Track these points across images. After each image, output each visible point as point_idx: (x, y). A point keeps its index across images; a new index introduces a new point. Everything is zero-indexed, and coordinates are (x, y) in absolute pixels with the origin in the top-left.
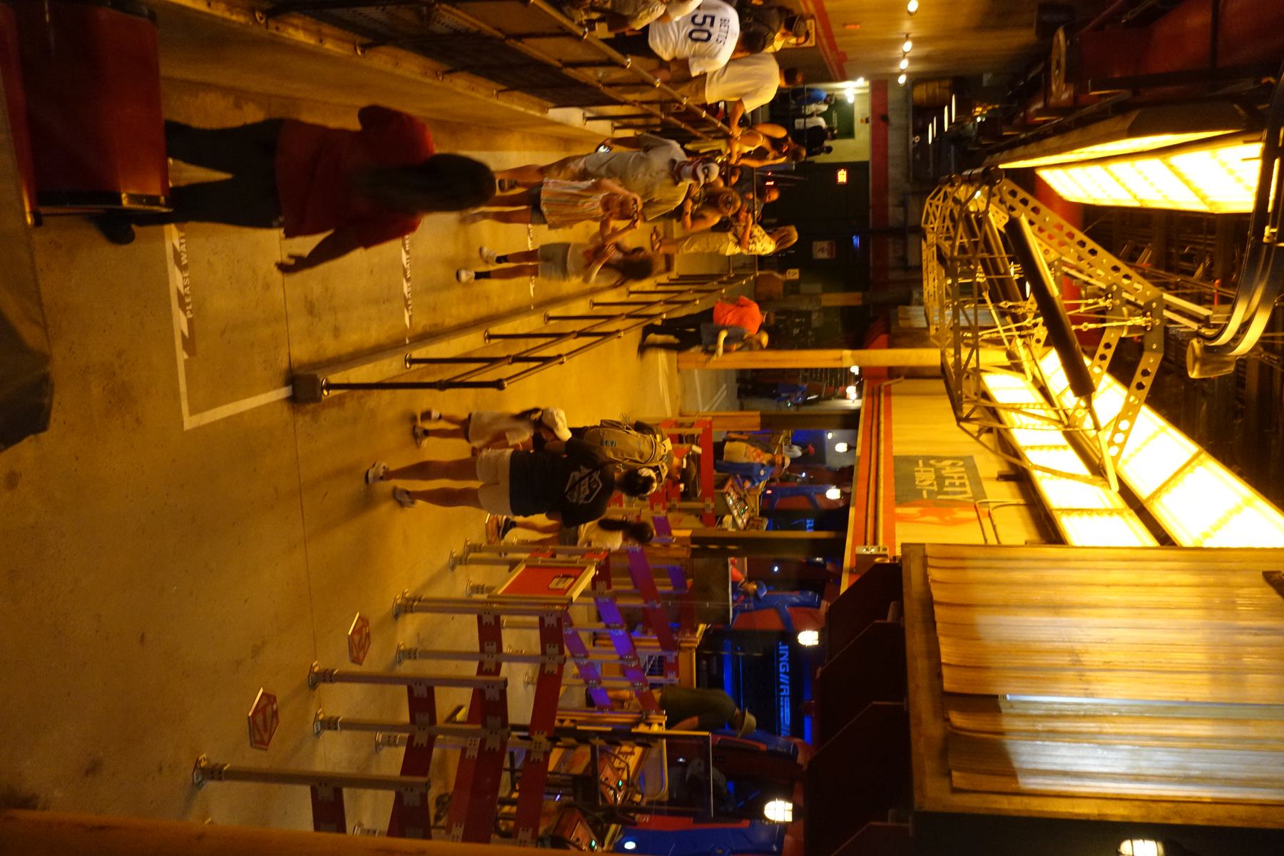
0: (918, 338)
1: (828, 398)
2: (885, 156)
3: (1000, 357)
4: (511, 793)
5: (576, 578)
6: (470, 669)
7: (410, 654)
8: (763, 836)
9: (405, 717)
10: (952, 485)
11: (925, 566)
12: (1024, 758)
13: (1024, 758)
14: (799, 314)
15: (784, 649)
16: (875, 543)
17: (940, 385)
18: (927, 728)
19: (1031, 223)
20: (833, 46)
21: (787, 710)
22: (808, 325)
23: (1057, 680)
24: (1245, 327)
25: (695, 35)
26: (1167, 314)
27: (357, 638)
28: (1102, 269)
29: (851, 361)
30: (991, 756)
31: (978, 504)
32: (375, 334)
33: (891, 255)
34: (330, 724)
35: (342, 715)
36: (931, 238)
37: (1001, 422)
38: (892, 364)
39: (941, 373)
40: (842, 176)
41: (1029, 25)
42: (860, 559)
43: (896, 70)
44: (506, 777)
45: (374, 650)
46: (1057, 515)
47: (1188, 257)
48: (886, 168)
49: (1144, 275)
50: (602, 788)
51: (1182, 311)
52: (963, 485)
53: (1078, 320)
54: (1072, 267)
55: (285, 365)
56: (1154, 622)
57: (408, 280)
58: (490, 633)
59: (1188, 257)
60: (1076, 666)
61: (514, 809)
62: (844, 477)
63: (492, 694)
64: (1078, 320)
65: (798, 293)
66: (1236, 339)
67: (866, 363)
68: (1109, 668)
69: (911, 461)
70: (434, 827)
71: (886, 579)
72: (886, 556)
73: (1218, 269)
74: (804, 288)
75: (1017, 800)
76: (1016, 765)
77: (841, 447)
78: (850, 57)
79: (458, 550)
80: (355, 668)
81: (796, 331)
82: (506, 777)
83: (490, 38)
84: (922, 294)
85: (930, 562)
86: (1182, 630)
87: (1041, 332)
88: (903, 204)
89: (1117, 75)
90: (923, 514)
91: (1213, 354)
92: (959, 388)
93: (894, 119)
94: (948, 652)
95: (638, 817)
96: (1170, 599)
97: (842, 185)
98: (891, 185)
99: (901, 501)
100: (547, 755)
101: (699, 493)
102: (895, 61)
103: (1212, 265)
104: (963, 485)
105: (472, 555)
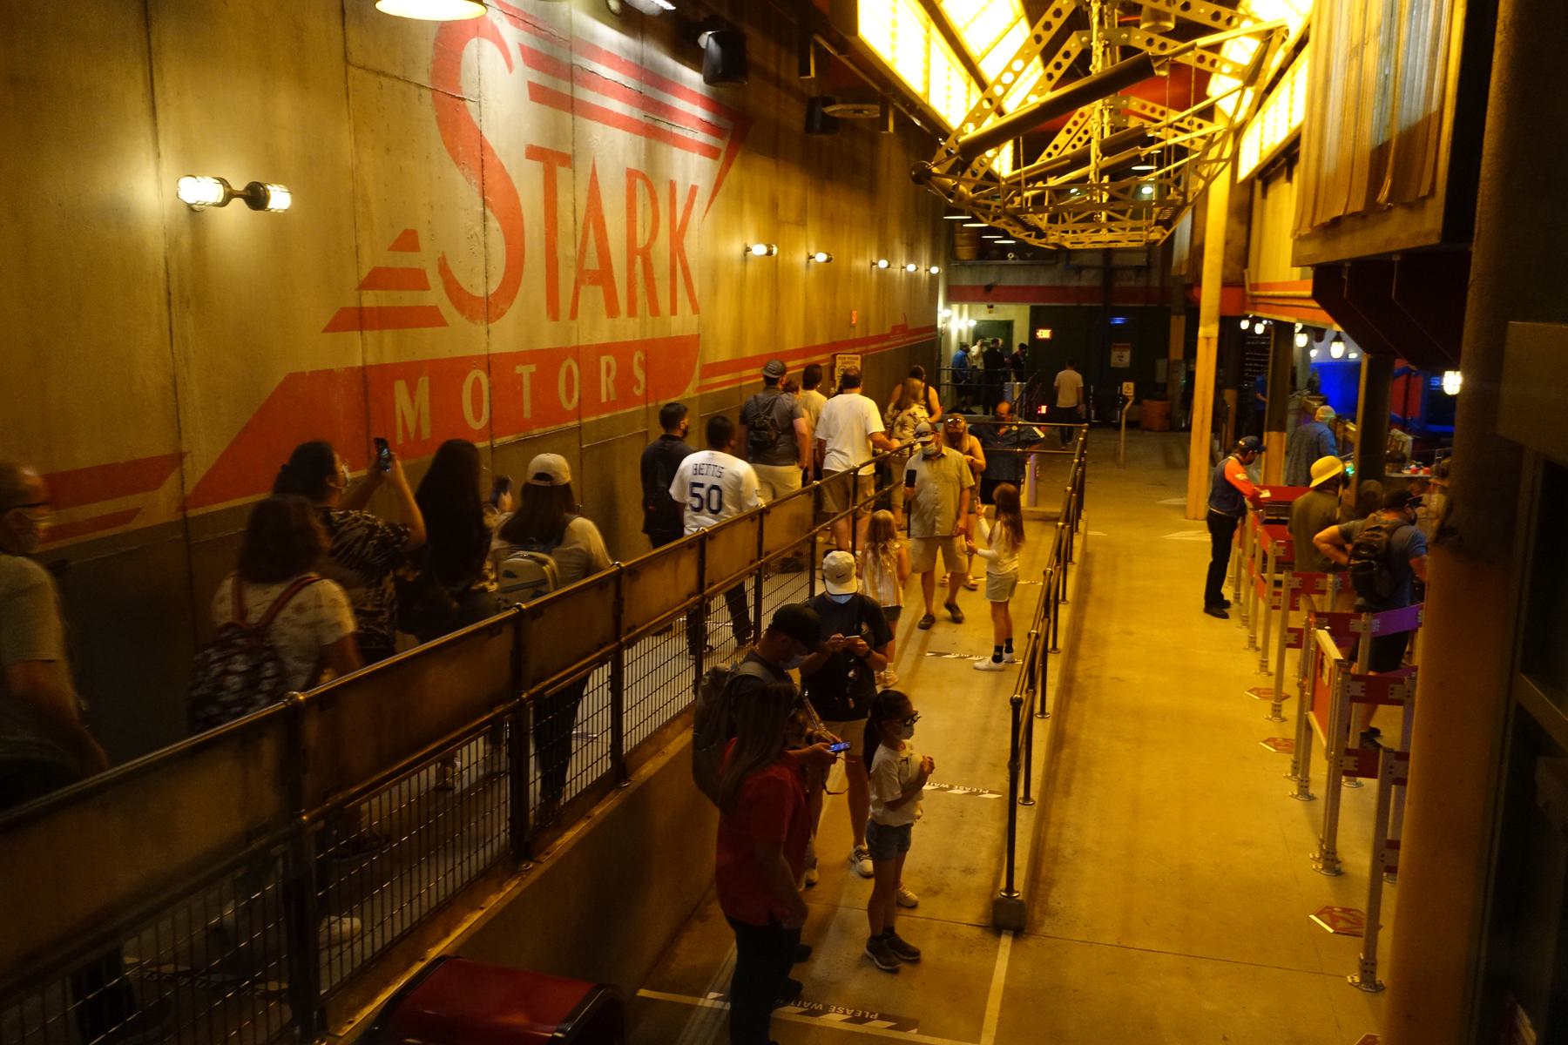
25: (714, 507)
27: (1342, 924)
32: (992, 832)
33: (1132, 283)
38: (1218, 283)
40: (1044, 334)
48: (1040, 287)
55: (977, 932)
57: (951, 787)
65: (1165, 385)
78: (900, 322)
88: (1079, 270)
97: (1052, 334)
98: (1058, 283)
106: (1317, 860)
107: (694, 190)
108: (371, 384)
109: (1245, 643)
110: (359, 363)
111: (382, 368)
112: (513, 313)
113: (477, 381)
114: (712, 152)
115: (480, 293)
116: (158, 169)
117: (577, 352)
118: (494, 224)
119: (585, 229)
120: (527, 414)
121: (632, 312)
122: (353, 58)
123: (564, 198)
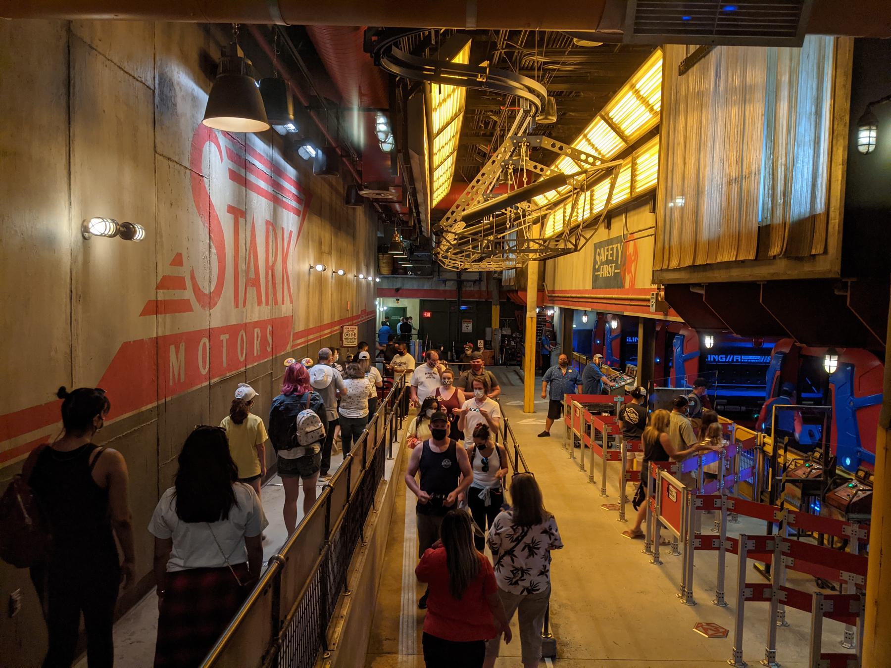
0: (522, 274)
1: (553, 326)
2: (417, 290)
3: (536, 228)
4: (814, 538)
5: (670, 484)
6: (732, 559)
7: (720, 597)
8: (841, 376)
9: (766, 605)
10: (612, 255)
11: (668, 270)
12: (803, 211)
13: (803, 211)
14: (503, 341)
15: (710, 358)
16: (649, 300)
17: (549, 263)
18: (782, 270)
19: (464, 210)
20: (358, 317)
21: (750, 357)
22: (509, 337)
23: (748, 192)
24: (531, 91)
26: (520, 134)
27: (710, 632)
28: (491, 172)
29: (532, 313)
30: (801, 231)
31: (624, 240)
34: (771, 656)
35: (763, 648)
36: (467, 266)
37: (578, 226)
39: (543, 261)
40: (427, 314)
41: (354, 209)
42: (659, 307)
43: (372, 283)
44: (802, 539)
45: (718, 622)
46: (634, 195)
47: (486, 124)
49: (495, 149)
50: (810, 477)
51: (521, 123)
52: (612, 249)
53: (521, 184)
54: (488, 188)
56: (709, 136)
58: (707, 543)
59: (486, 124)
60: (738, 180)
61: (826, 536)
62: (602, 318)
63: (751, 545)
64: (521, 184)
66: (538, 95)
67: (535, 304)
68: (740, 161)
69: (595, 279)
70: (841, 592)
71: (675, 294)
72: (657, 294)
73: (494, 108)
74: (488, 338)
75: (832, 214)
76: (807, 215)
77: (585, 319)
78: (364, 308)
79: (649, 558)
80: (732, 635)
81: (513, 343)
82: (802, 539)
83: (347, 512)
84: (495, 272)
85: (665, 267)
86: (716, 120)
87: (524, 205)
89: (389, 163)
90: (630, 272)
91: (544, 110)
92: (552, 252)
93: (398, 286)
94: (727, 256)
95: (831, 455)
96: (695, 127)
97: (432, 314)
99: (621, 285)
100: (790, 512)
101: (611, 404)
102: (368, 283)
103: (492, 111)
104: (612, 249)
105: (653, 549)
106: (681, 598)
107: (291, 232)
108: (159, 345)
109: (587, 480)
110: (155, 336)
111: (165, 337)
112: (220, 303)
113: (205, 343)
114: (297, 212)
115: (207, 292)
116: (70, 212)
117: (245, 326)
118: (214, 250)
119: (250, 254)
120: (225, 365)
121: (267, 304)
122: (158, 150)
123: (242, 236)
